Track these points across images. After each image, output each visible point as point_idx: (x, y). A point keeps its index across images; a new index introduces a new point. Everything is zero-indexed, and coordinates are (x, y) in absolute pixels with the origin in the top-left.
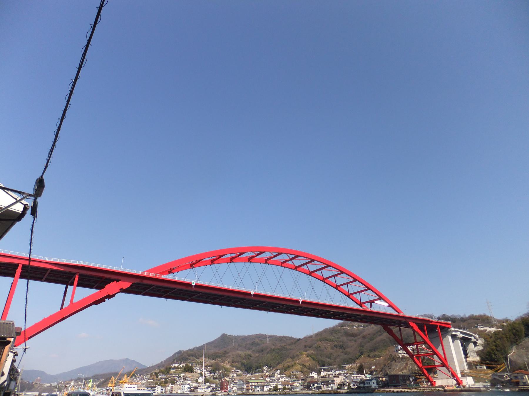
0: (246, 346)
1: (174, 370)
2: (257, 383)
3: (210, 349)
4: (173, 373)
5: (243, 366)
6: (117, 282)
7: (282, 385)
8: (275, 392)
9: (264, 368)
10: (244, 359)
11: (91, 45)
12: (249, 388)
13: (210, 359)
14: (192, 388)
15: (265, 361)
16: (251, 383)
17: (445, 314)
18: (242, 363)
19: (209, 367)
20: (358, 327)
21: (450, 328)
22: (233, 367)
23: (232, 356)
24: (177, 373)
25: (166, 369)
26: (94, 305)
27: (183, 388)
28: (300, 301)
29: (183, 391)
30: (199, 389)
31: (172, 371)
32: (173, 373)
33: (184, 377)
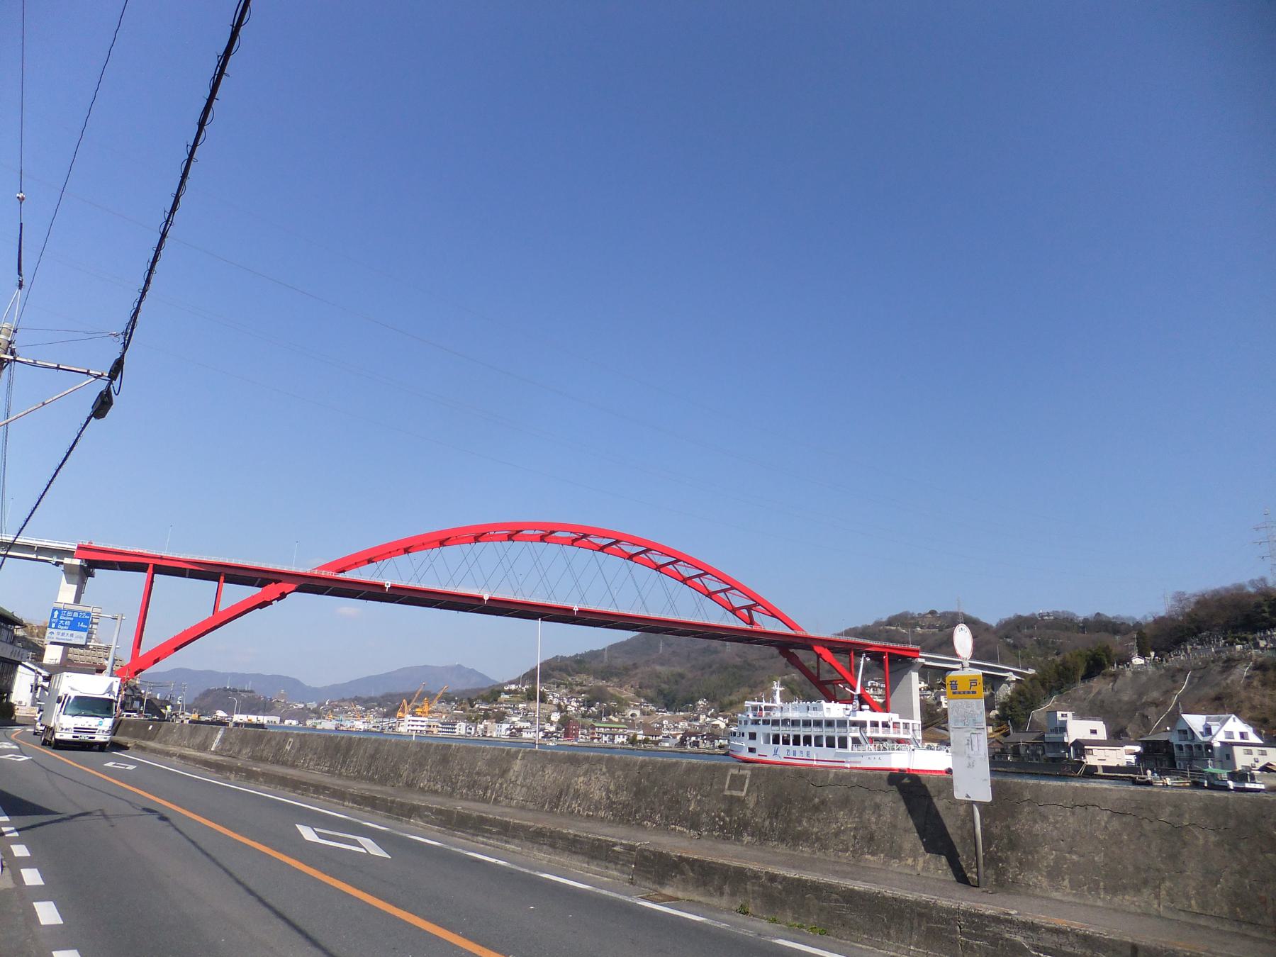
0: (689, 656)
1: (507, 697)
2: (611, 728)
3: (616, 658)
4: (505, 701)
5: (662, 697)
6: (276, 583)
7: (643, 735)
8: (630, 746)
9: (700, 702)
10: (665, 683)
11: (217, 99)
12: (595, 736)
13: (597, 678)
14: (514, 731)
15: (703, 689)
16: (599, 727)
17: (1101, 612)
18: (659, 690)
19: (584, 693)
20: (928, 628)
21: (915, 658)
22: (639, 697)
23: (640, 675)
24: (513, 701)
25: (492, 693)
26: (258, 609)
27: (499, 729)
28: (574, 609)
29: (499, 733)
30: (525, 732)
31: (504, 697)
32: (505, 701)
33: (524, 709)
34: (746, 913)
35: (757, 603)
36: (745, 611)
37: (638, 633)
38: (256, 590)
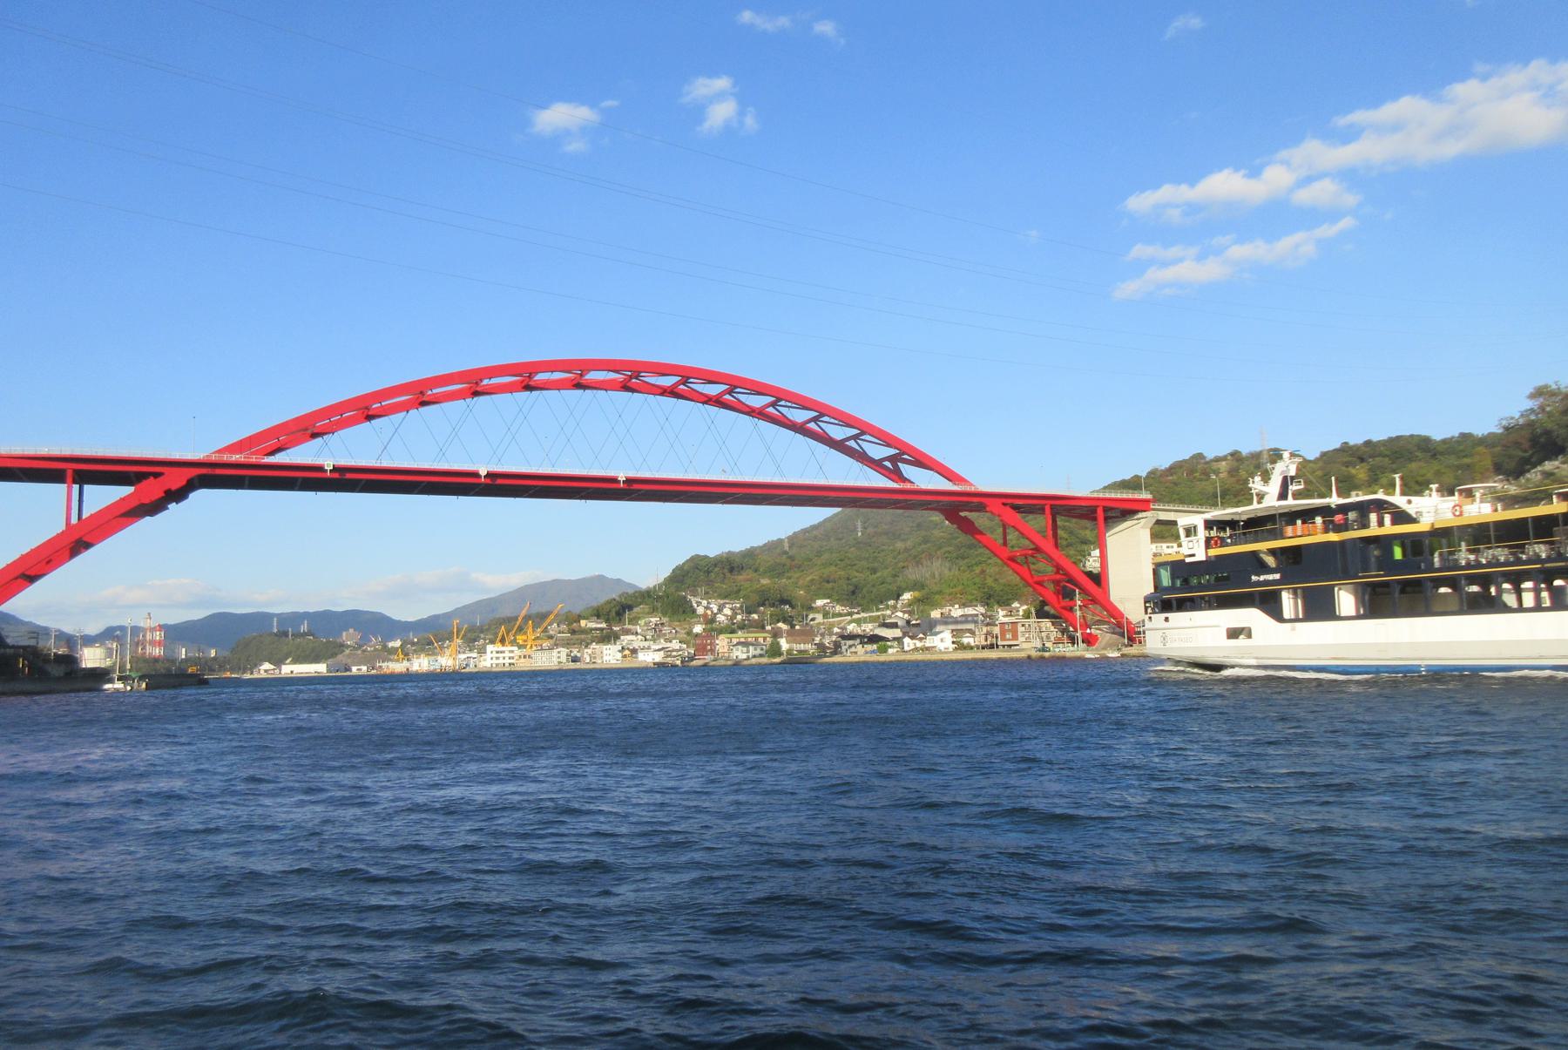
34: (1103, 765)
35: (908, 454)
36: (887, 464)
37: (840, 509)
38: (127, 490)
